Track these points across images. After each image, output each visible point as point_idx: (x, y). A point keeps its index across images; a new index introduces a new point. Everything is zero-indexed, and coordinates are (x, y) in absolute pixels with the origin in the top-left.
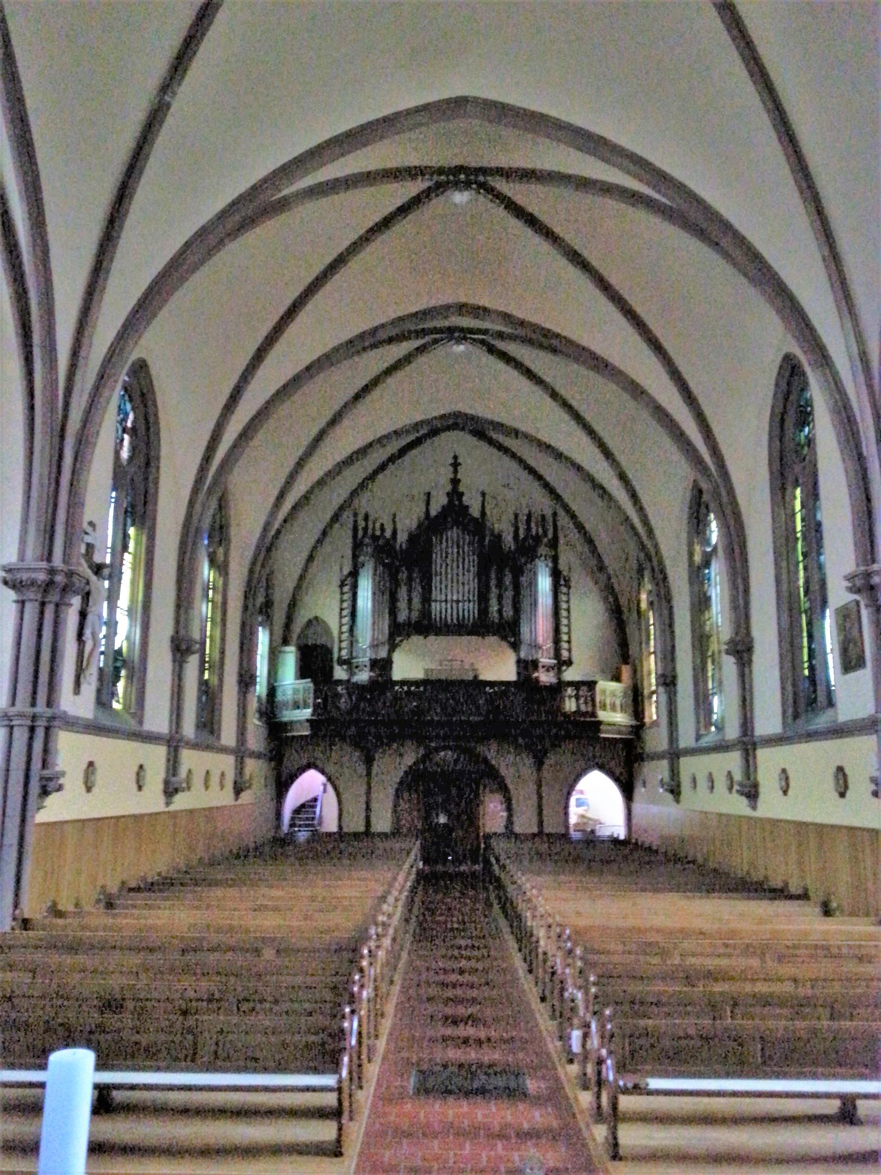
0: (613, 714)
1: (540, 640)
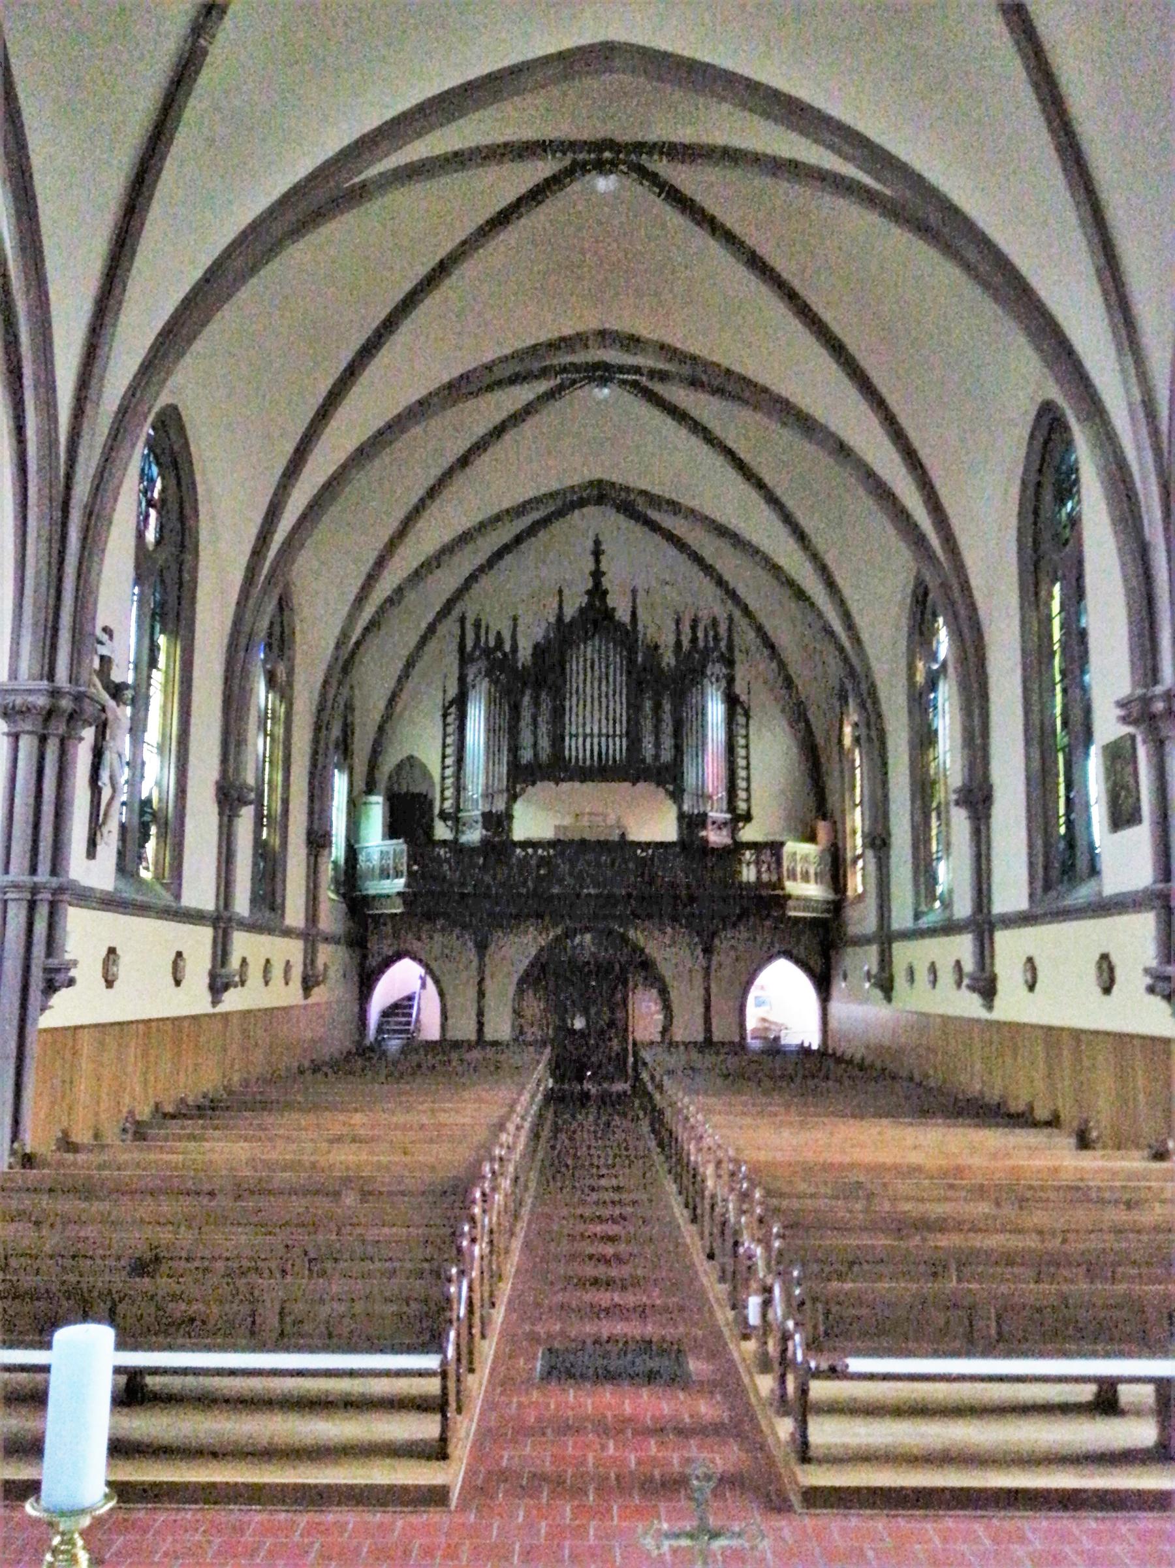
0: (804, 885)
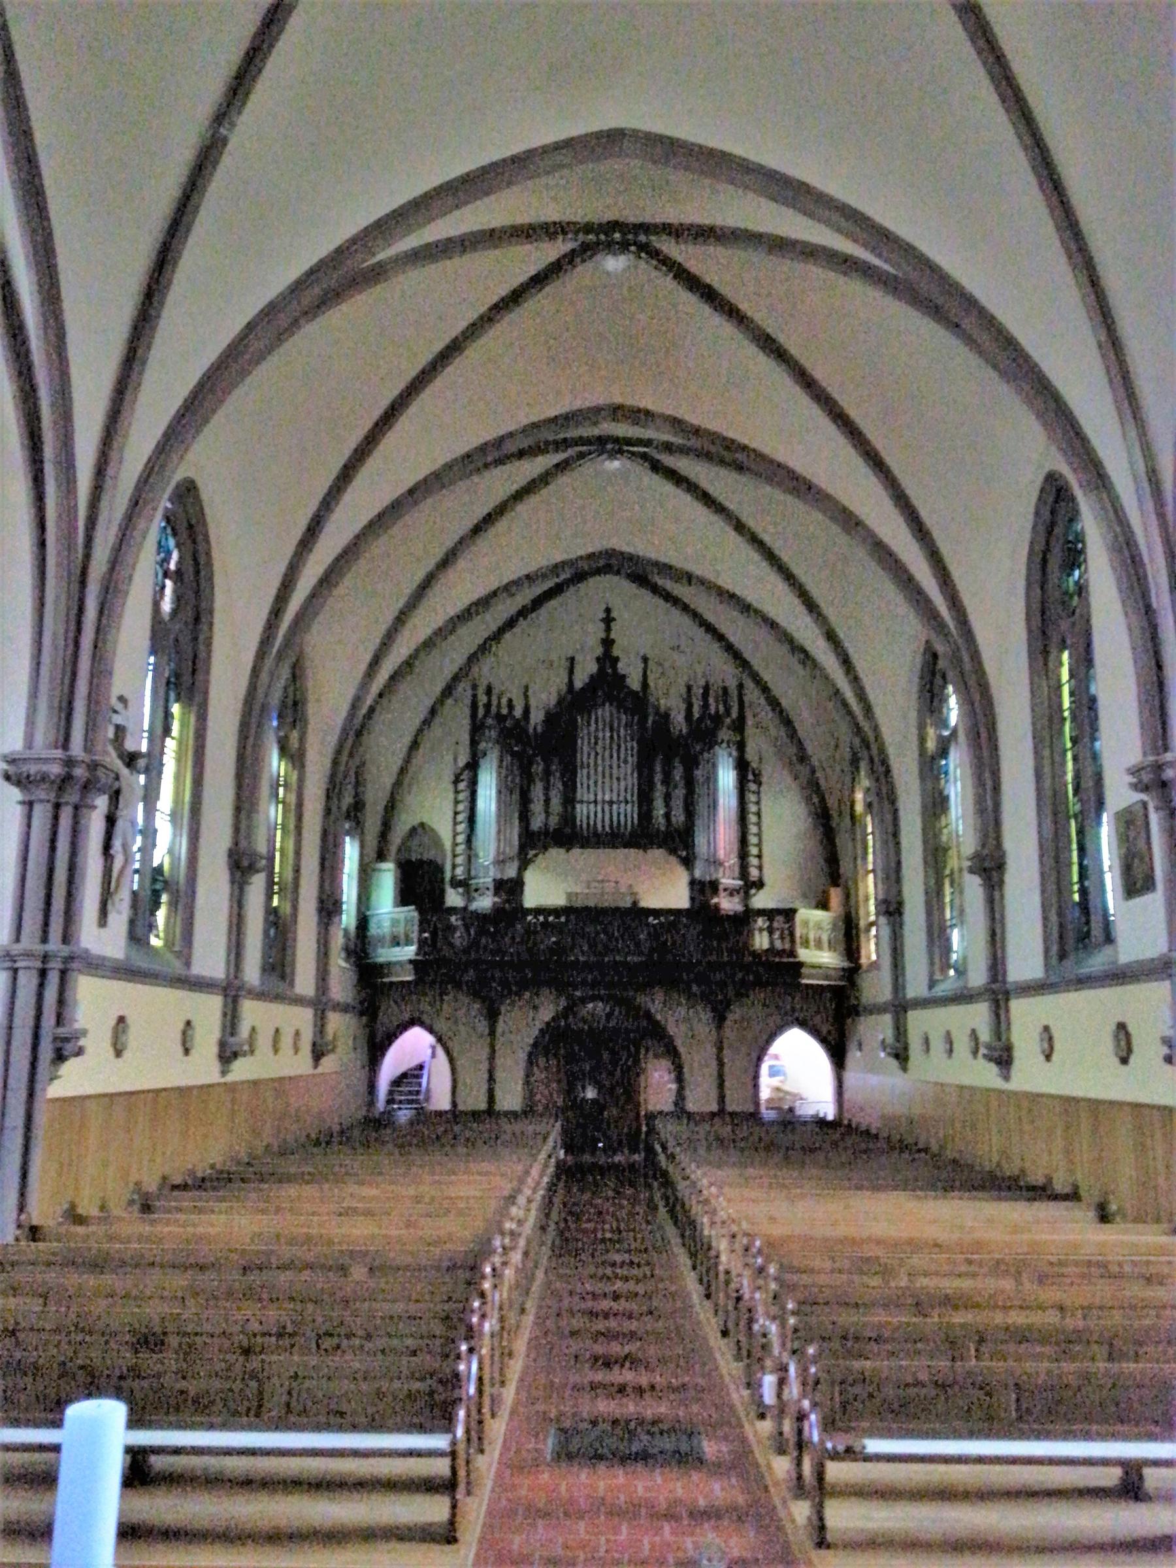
0: (818, 953)
1: (721, 854)
